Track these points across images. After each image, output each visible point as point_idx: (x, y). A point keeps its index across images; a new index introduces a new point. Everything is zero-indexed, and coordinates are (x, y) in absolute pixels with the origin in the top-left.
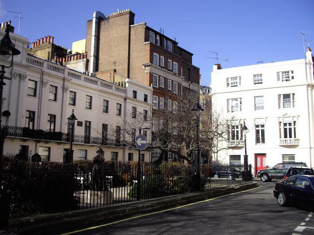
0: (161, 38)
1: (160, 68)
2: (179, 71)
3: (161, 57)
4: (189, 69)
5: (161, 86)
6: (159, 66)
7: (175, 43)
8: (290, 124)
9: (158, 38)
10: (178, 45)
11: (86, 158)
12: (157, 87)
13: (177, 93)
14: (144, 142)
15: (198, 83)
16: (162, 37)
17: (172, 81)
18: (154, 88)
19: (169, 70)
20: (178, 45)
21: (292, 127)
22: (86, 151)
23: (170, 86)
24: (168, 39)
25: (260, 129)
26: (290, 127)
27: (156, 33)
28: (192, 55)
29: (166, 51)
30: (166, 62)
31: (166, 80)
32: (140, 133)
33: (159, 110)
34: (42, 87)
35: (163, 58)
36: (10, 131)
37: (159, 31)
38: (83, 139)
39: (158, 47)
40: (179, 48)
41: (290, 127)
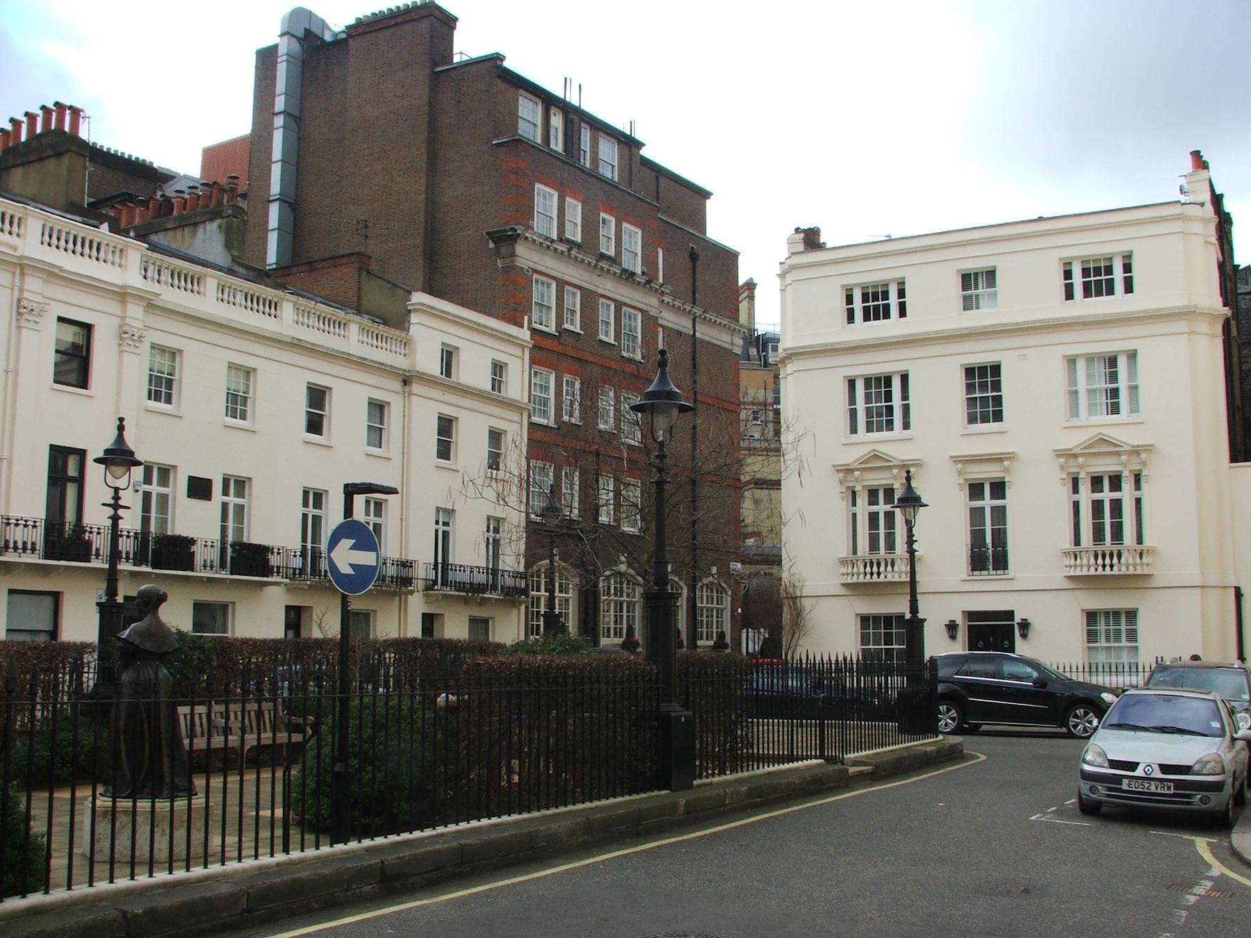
0: (568, 124)
1: (562, 247)
2: (649, 260)
3: (568, 199)
4: (693, 257)
5: (567, 326)
6: (561, 240)
7: (629, 143)
8: (1116, 482)
9: (557, 121)
10: (643, 152)
11: (54, 633)
12: (552, 329)
13: (638, 357)
14: (367, 558)
15: (738, 321)
16: (575, 117)
17: (619, 305)
18: (534, 331)
19: (603, 257)
20: (643, 152)
21: (1127, 494)
22: (56, 597)
23: (573, 312)
24: (600, 128)
25: (987, 502)
26: (1115, 495)
27: (548, 101)
28: (705, 195)
29: (594, 175)
30: (591, 227)
31: (590, 299)
32: (348, 511)
33: (562, 429)
34: (19, 334)
35: (613, 220)
36: (274, 560)
37: (556, 90)
38: (38, 536)
39: (553, 155)
40: (646, 162)
41: (1115, 495)
